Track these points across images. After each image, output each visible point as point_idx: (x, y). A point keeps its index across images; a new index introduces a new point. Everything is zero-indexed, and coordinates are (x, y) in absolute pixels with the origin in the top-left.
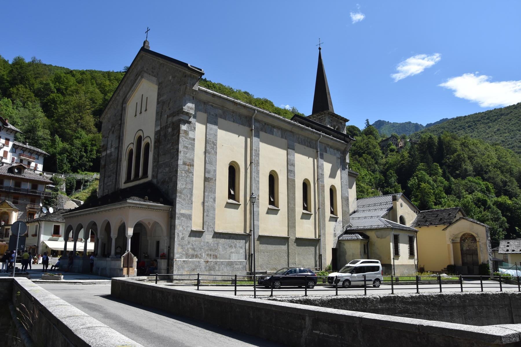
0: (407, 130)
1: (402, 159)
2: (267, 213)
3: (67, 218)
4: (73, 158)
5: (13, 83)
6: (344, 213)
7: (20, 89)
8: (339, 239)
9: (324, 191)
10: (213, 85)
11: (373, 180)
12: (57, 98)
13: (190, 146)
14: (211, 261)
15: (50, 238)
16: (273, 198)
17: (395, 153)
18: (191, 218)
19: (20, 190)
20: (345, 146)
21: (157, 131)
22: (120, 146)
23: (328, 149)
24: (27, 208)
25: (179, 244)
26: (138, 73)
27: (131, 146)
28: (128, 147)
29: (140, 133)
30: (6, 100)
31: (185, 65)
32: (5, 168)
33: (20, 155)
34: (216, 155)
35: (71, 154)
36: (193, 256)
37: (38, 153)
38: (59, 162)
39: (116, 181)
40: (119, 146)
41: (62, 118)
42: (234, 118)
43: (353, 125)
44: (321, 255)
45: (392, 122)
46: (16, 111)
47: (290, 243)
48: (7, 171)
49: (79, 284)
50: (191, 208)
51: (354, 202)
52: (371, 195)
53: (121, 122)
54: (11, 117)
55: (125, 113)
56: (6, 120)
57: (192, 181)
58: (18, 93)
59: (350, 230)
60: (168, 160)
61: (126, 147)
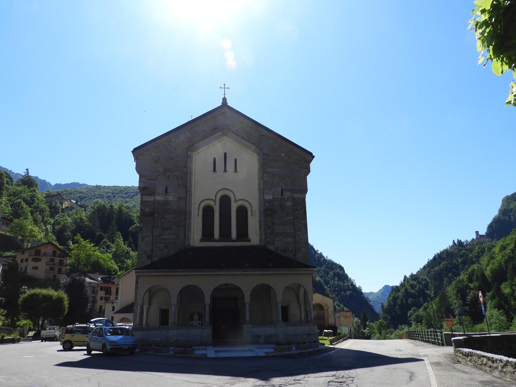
45: (16, 172)
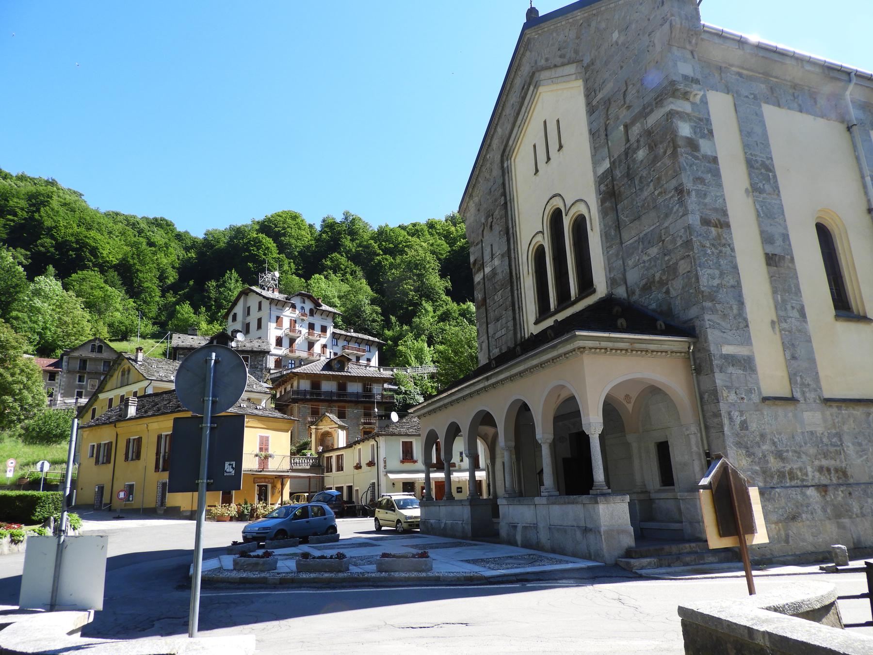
3: (424, 415)
26: (525, 81)
27: (539, 238)
28: (530, 244)
29: (558, 203)
34: (779, 194)
39: (515, 325)
42: (800, 102)
55: (510, 179)
56: (318, 299)
61: (525, 247)
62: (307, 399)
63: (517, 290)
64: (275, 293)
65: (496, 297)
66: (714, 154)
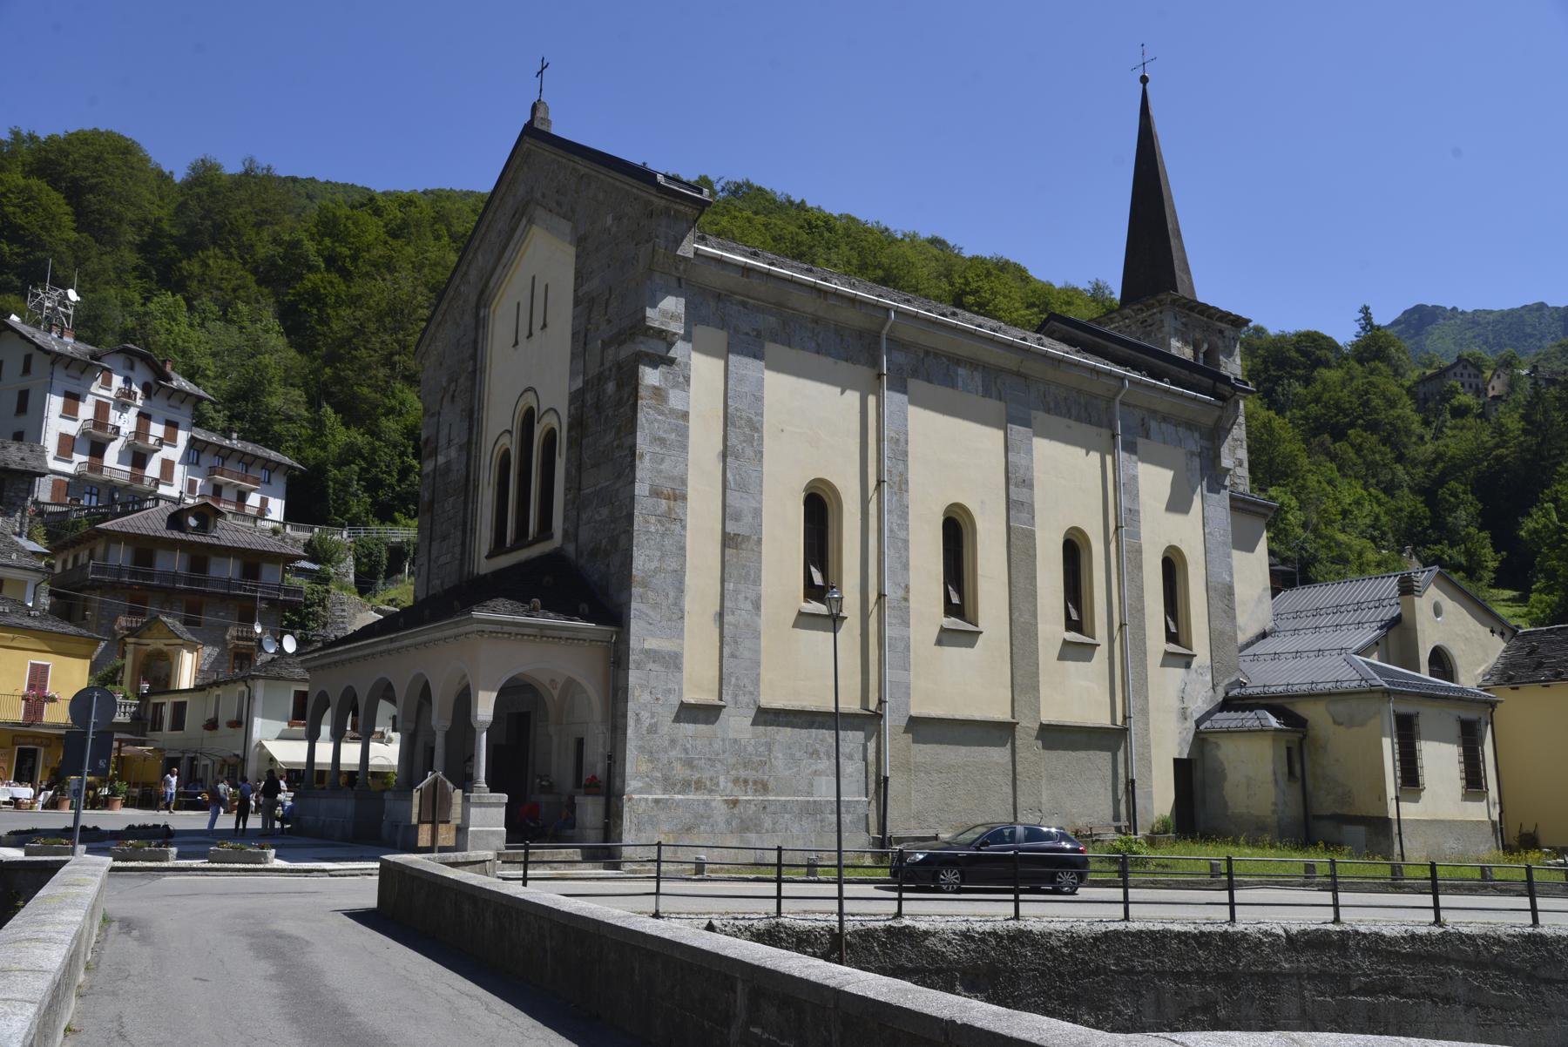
0: (1531, 336)
1: (1497, 439)
2: (939, 642)
3: (315, 668)
4: (381, 476)
5: (189, 246)
6: (1217, 640)
7: (211, 262)
8: (1198, 727)
9: (1140, 568)
10: (826, 222)
11: (1387, 518)
12: (325, 288)
13: (673, 436)
14: (747, 801)
15: (283, 730)
16: (960, 592)
17: (1470, 420)
18: (681, 664)
19: (205, 582)
20: (1217, 413)
21: (575, 392)
22: (474, 441)
23: (1153, 424)
24: (228, 637)
25: (641, 749)
27: (505, 440)
28: (496, 443)
29: (530, 400)
30: (168, 298)
31: (644, 175)
32: (158, 517)
33: (213, 471)
35: (372, 463)
36: (686, 786)
37: (269, 464)
38: (334, 489)
39: (463, 553)
40: (469, 442)
41: (342, 351)
42: (820, 341)
43: (1312, 329)
44: (1133, 781)
45: (1469, 310)
46: (198, 334)
47: (1018, 743)
48: (165, 526)
49: (319, 874)
50: (680, 634)
51: (1260, 600)
52: (1374, 572)
53: (475, 365)
54: (184, 353)
56: (164, 362)
57: (683, 548)
58: (204, 274)
59: (1240, 699)
60: (607, 483)
62: (123, 583)
63: (473, 503)
64: (66, 339)
65: (446, 505)
66: (685, 409)
